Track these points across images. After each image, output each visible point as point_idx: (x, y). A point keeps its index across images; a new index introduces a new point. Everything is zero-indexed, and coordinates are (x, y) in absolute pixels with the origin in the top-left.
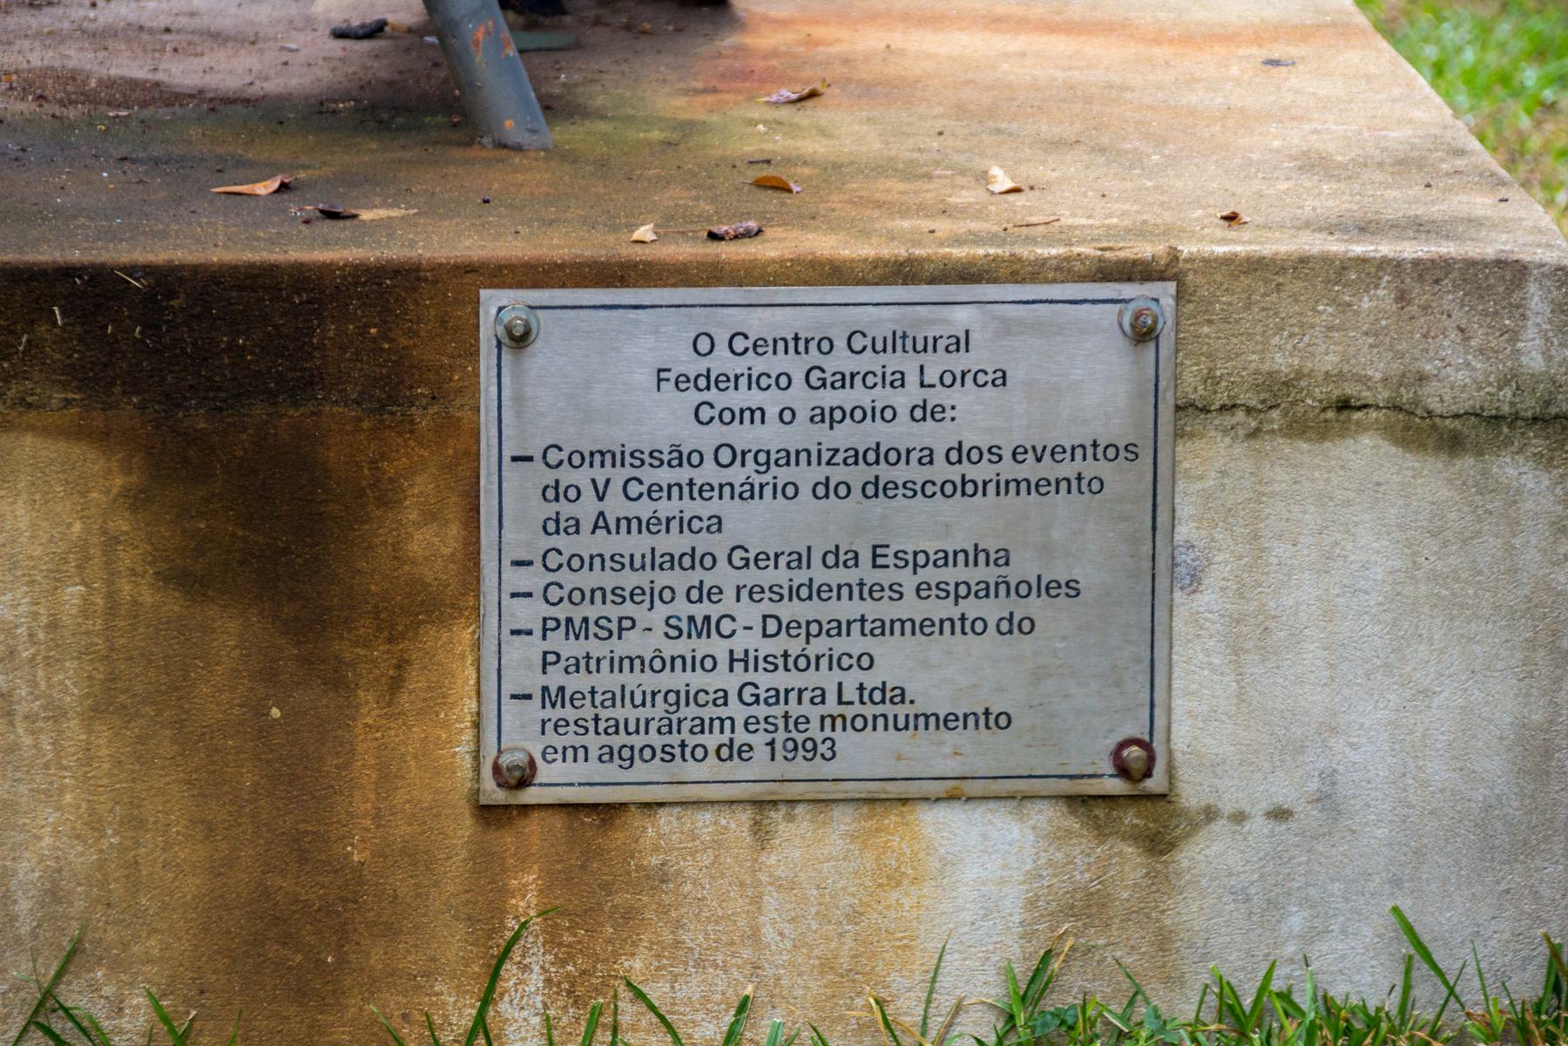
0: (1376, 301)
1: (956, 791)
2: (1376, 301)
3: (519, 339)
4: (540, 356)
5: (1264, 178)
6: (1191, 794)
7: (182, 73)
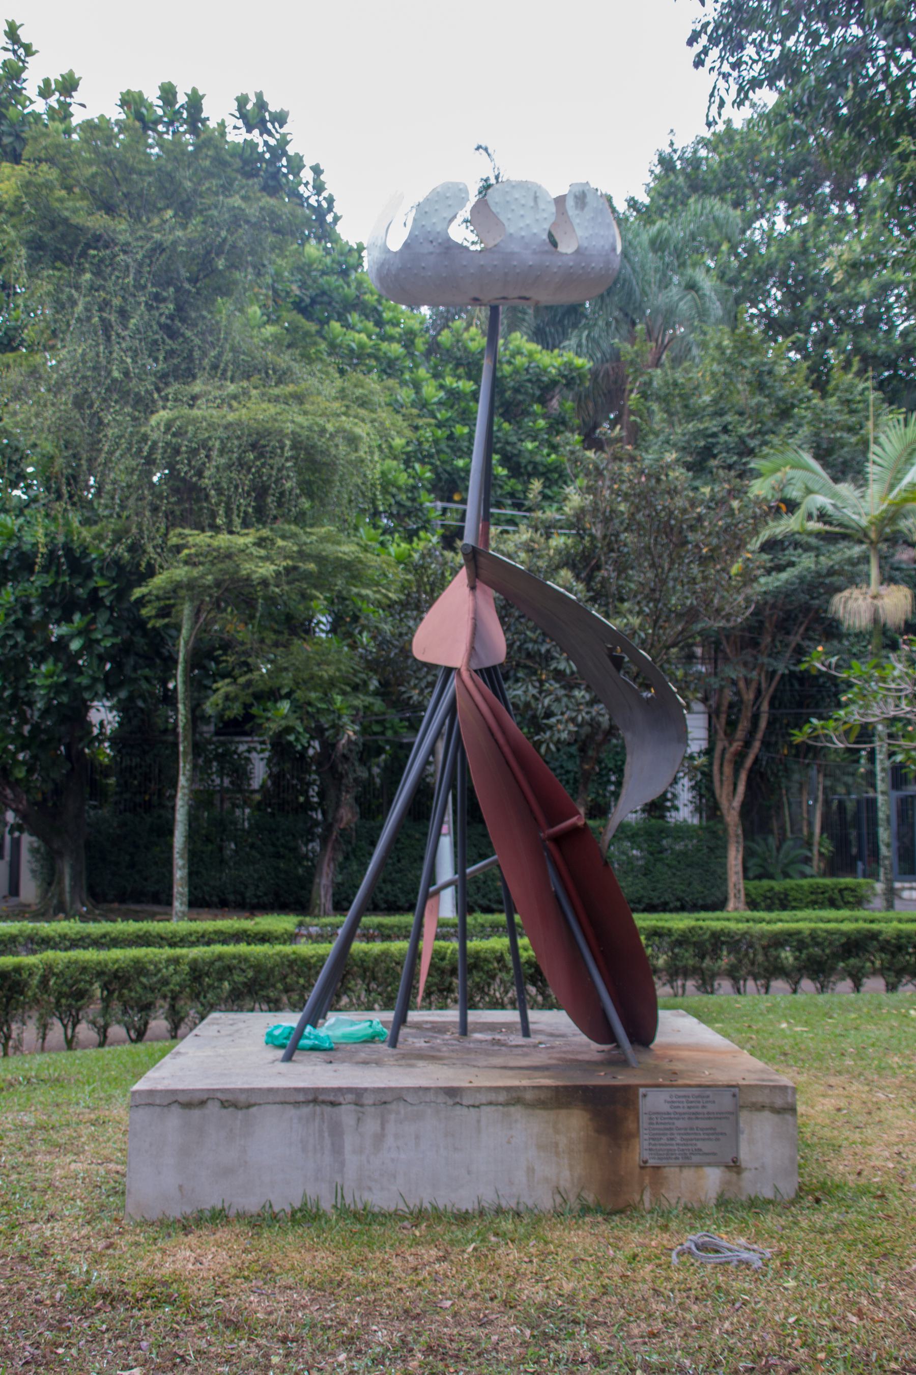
0: (767, 1091)
1: (710, 1165)
2: (767, 1091)
3: (645, 1096)
4: (649, 1098)
5: (729, 1263)
6: (744, 1165)
7: (580, 1057)
